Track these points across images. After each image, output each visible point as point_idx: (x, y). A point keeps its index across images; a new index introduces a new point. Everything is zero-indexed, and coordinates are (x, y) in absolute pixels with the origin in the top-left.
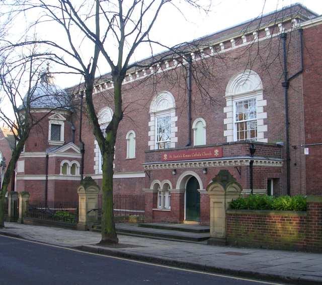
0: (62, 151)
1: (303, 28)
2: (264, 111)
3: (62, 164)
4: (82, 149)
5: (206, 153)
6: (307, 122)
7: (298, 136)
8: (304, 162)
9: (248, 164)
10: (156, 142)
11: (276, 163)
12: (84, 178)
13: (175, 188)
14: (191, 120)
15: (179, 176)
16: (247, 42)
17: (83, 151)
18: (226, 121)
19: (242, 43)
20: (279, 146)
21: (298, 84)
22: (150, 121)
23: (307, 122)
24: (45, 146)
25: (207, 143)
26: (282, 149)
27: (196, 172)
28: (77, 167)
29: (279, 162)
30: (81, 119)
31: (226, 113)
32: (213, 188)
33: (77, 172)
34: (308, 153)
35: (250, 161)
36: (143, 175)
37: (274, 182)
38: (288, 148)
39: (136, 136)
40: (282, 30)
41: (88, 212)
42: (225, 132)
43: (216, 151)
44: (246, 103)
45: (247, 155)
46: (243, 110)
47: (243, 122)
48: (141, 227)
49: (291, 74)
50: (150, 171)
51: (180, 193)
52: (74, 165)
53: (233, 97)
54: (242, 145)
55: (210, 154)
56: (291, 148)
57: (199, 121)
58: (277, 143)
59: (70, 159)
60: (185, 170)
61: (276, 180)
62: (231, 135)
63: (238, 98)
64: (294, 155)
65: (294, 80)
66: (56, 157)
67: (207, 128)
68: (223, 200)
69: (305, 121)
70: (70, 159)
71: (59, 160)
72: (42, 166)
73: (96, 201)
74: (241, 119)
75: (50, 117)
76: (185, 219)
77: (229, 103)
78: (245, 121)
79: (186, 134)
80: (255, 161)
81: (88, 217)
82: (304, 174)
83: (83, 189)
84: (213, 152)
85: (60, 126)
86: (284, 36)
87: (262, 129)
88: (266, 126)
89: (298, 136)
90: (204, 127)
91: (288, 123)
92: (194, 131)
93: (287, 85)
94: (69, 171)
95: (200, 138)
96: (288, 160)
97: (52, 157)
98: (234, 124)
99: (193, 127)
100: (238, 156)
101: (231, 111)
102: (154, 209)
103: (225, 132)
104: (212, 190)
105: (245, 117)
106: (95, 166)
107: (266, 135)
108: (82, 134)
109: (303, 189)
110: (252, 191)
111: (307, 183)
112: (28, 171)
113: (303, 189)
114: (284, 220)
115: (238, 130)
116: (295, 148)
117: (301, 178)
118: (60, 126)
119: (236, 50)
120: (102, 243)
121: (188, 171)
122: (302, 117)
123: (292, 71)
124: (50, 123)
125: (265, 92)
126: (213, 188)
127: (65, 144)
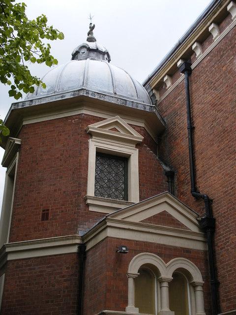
0: (137, 219)
3: (134, 267)
17: (208, 226)
52: (181, 277)
59: (167, 253)
70: (167, 253)
75: (94, 127)
85: (124, 159)
108: (198, 173)
118: (124, 159)
124: (93, 145)
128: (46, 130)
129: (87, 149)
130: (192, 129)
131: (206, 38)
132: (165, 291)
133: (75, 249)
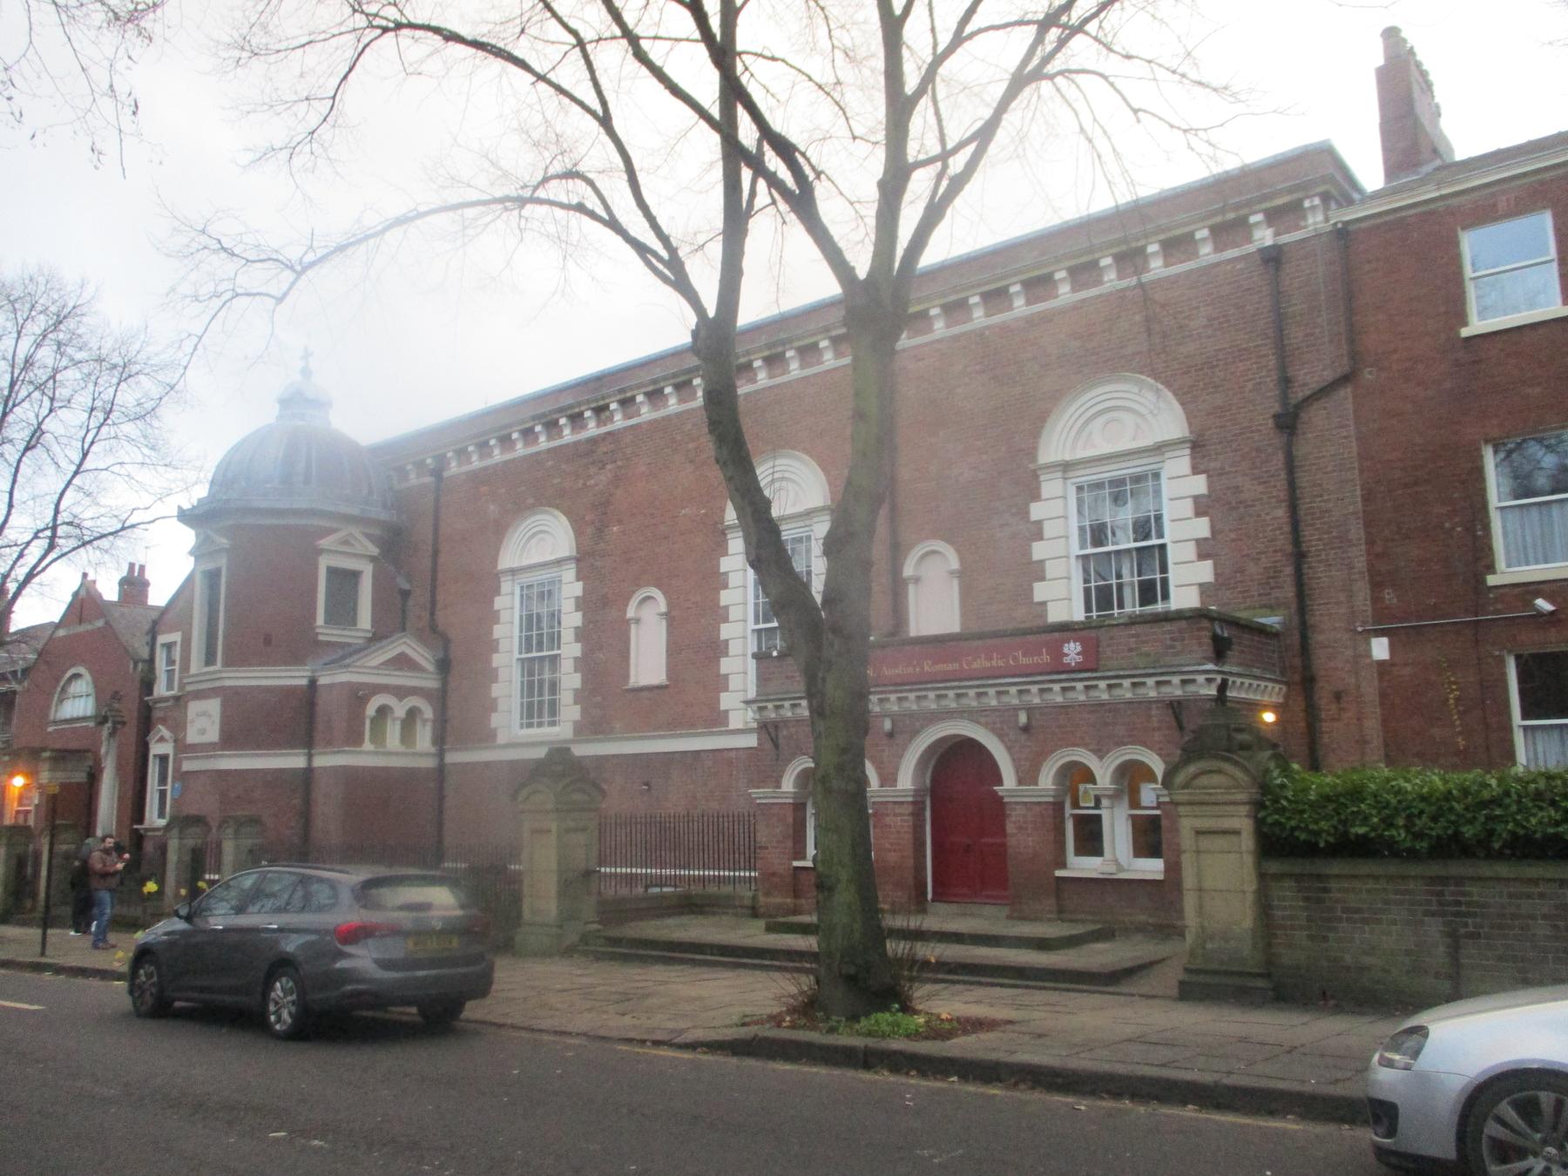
0: (374, 663)
1: (1351, 228)
2: (1198, 514)
4: (441, 655)
5: (1024, 655)
8: (1370, 688)
10: (516, 655)
13: (894, 782)
15: (904, 748)
16: (1166, 266)
17: (444, 666)
18: (725, 597)
19: (1099, 282)
22: (726, 554)
23: (1378, 549)
25: (963, 624)
27: (986, 725)
28: (425, 721)
31: (1039, 523)
32: (1196, 776)
33: (424, 738)
35: (1219, 678)
39: (670, 604)
40: (1265, 237)
42: (723, 626)
45: (1208, 660)
49: (1304, 385)
50: (776, 725)
51: (913, 803)
52: (412, 714)
53: (1066, 467)
55: (1046, 658)
57: (934, 552)
59: (401, 692)
60: (949, 714)
62: (1063, 597)
63: (1087, 471)
64: (1332, 664)
66: (350, 684)
67: (669, 617)
69: (1370, 542)
70: (401, 692)
74: (1147, 537)
75: (324, 543)
76: (930, 896)
77: (506, 586)
82: (1372, 725)
84: (1058, 654)
85: (355, 575)
86: (1273, 258)
88: (1209, 564)
90: (952, 573)
91: (1299, 556)
92: (633, 627)
93: (1288, 423)
94: (393, 733)
97: (331, 686)
98: (1073, 560)
99: (908, 570)
101: (1059, 520)
103: (723, 626)
104: (1186, 786)
112: (232, 738)
115: (1086, 581)
118: (355, 575)
119: (1076, 307)
120: (808, 1008)
121: (966, 723)
122: (1356, 531)
123: (1310, 375)
124: (324, 563)
125: (1197, 446)
126: (1196, 776)
127: (378, 636)
128: (19, 833)
129: (316, 567)
132: (398, 727)
133: (304, 682)
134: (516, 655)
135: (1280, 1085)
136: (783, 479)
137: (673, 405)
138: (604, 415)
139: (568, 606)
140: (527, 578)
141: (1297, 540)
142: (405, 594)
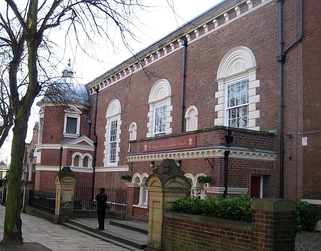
3: (74, 156)
6: (307, 103)
7: (295, 122)
8: (301, 156)
9: (223, 156)
11: (268, 157)
12: (62, 169)
14: (184, 108)
17: (96, 144)
18: (217, 108)
20: (272, 135)
21: (295, 57)
23: (307, 103)
24: (62, 139)
26: (275, 138)
29: (269, 155)
30: (96, 112)
32: (153, 182)
34: (306, 144)
35: (224, 151)
36: (127, 169)
37: (264, 180)
38: (282, 138)
41: (62, 205)
43: (191, 140)
44: (239, 84)
46: (236, 95)
47: (235, 108)
48: (112, 224)
52: (86, 158)
53: (224, 79)
54: (215, 132)
56: (286, 138)
58: (270, 132)
59: (83, 152)
61: (266, 177)
63: (240, 77)
65: (291, 52)
67: (199, 116)
68: (161, 199)
69: (304, 102)
70: (83, 152)
71: (71, 152)
72: (57, 157)
73: (72, 193)
77: (220, 87)
78: (237, 106)
79: (180, 120)
80: (232, 152)
81: (62, 210)
82: (300, 171)
83: (159, 183)
87: (254, 114)
89: (295, 122)
91: (283, 107)
94: (81, 162)
95: (192, 125)
96: (282, 153)
100: (212, 145)
102: (134, 205)
105: (237, 103)
106: (119, 160)
107: (258, 122)
108: (96, 127)
109: (299, 190)
110: (226, 190)
111: (304, 182)
112: (44, 163)
113: (299, 190)
114: (224, 233)
116: (290, 136)
117: (297, 176)
119: (230, 25)
122: (300, 98)
123: (290, 41)
126: (153, 182)
130: (96, 108)
131: (123, 63)
134: (109, 142)
135: (89, 226)
136: (238, 59)
137: (173, 50)
138: (232, 14)
139: (252, 92)
140: (230, 82)
141: (283, 102)
142: (90, 124)
